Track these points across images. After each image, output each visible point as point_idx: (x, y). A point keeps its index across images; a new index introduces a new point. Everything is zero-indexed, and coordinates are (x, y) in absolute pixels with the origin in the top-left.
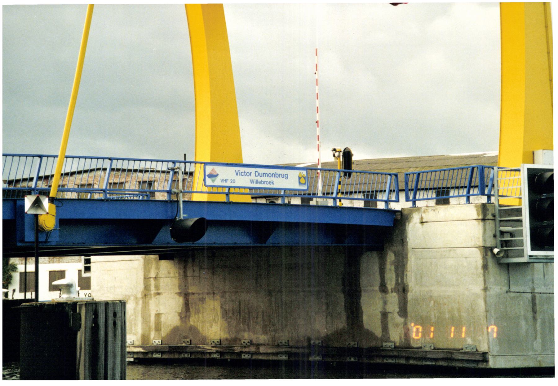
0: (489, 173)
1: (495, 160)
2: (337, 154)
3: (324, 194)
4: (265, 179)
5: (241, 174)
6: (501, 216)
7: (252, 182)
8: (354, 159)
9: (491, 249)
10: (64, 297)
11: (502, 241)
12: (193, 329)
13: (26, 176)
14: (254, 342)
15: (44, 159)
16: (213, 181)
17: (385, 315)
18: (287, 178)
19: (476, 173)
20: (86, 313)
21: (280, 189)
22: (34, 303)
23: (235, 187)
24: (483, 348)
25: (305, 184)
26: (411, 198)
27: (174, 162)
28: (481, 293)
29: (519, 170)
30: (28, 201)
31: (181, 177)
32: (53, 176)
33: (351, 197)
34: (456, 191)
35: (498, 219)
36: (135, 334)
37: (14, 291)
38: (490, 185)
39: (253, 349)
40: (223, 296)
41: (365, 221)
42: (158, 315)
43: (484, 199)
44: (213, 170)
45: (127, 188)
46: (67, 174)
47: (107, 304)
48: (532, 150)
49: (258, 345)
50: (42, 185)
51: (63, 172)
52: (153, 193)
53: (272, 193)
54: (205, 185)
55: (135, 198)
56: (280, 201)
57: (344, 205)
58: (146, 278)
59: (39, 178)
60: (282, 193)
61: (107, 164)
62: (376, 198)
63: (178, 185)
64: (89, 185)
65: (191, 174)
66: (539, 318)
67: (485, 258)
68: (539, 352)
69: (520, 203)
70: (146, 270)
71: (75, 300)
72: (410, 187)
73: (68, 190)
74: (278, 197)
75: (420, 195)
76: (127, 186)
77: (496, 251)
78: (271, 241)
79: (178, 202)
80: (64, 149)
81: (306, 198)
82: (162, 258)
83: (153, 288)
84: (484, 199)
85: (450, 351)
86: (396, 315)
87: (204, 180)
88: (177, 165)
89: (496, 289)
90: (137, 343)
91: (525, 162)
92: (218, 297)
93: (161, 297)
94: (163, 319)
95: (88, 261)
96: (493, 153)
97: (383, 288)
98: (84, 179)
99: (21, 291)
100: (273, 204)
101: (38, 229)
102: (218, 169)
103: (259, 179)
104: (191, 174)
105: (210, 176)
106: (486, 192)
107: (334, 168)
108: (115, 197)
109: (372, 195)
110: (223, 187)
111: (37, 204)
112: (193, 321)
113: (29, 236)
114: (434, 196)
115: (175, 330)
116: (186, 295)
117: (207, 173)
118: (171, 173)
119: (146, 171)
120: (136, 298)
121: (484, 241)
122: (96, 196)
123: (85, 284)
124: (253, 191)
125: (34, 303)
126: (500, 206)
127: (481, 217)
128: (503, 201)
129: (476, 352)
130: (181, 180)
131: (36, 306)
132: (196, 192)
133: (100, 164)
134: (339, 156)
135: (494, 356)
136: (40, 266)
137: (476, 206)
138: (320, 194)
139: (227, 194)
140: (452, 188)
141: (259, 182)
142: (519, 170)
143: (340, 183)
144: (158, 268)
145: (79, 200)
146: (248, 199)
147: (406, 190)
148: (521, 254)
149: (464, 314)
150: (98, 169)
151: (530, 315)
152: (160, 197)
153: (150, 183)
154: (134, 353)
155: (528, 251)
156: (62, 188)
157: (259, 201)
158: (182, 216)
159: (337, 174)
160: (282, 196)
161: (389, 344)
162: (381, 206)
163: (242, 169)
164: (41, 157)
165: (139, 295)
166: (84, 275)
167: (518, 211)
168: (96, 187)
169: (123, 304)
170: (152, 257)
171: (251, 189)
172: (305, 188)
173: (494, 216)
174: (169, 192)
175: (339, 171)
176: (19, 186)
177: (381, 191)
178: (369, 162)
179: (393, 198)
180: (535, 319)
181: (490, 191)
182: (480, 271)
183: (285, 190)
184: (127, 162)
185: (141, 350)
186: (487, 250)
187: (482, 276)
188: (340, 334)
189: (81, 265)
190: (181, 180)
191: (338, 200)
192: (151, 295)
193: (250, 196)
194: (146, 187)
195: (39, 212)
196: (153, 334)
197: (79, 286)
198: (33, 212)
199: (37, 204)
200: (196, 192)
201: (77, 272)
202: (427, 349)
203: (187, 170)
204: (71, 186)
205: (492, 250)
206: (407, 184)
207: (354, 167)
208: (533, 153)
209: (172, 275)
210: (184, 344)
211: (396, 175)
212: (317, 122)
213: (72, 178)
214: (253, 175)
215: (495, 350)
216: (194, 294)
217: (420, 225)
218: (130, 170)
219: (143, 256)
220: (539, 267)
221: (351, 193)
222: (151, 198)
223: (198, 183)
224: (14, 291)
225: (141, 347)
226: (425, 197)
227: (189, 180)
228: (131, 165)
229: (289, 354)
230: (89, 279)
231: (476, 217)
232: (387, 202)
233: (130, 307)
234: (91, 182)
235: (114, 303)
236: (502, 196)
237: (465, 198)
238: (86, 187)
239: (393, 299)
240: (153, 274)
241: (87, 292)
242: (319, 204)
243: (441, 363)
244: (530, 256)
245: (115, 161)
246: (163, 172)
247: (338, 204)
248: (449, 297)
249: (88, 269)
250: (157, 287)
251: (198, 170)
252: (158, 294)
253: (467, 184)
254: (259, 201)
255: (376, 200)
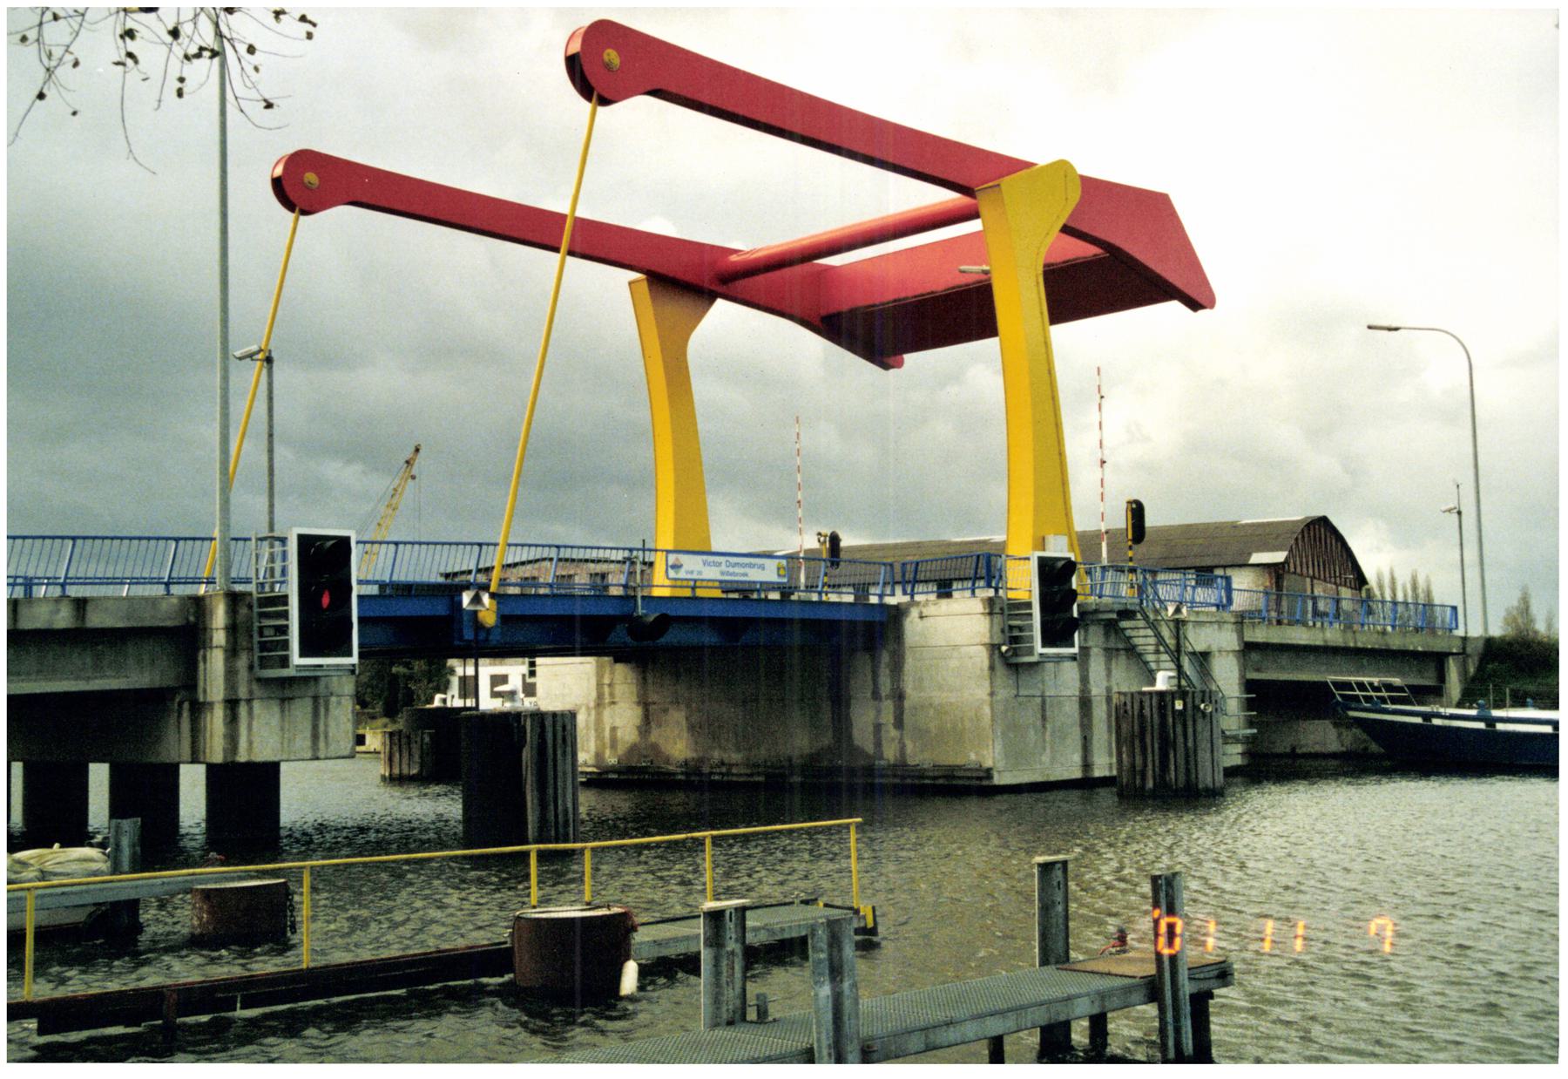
0: (996, 562)
1: (1003, 545)
2: (822, 539)
3: (807, 587)
4: (737, 570)
5: (709, 565)
6: (1009, 609)
7: (722, 573)
8: (843, 544)
9: (999, 647)
10: (508, 706)
11: (1010, 637)
12: (655, 747)
13: (464, 568)
14: (726, 762)
15: (484, 547)
16: (677, 573)
17: (878, 728)
18: (763, 569)
19: (982, 562)
20: (532, 725)
21: (754, 582)
22: (474, 712)
23: (702, 580)
24: (988, 763)
25: (784, 576)
26: (909, 591)
27: (631, 550)
28: (987, 698)
29: (1028, 559)
30: (466, 598)
31: (639, 567)
32: (493, 568)
33: (840, 590)
34: (960, 583)
35: (1006, 612)
36: (588, 752)
37: (453, 697)
38: (997, 577)
39: (724, 770)
40: (688, 706)
41: (860, 616)
42: (614, 729)
43: (991, 593)
44: (677, 559)
45: (576, 582)
46: (509, 566)
47: (554, 715)
48: (1042, 534)
49: (731, 765)
50: (482, 578)
51: (504, 563)
52: (606, 587)
53: (747, 586)
54: (668, 578)
55: (586, 593)
56: (755, 596)
57: (832, 600)
58: (600, 685)
59: (479, 571)
60: (758, 586)
61: (553, 553)
62: (868, 591)
63: (635, 578)
64: (534, 578)
65: (651, 564)
66: (1048, 726)
67: (991, 656)
68: (1047, 765)
69: (1030, 596)
70: (600, 676)
71: (519, 710)
72: (907, 579)
73: (510, 585)
74: (752, 591)
75: (920, 588)
76: (577, 579)
77: (1004, 648)
78: (744, 639)
79: (635, 597)
80: (506, 537)
81: (786, 591)
82: (617, 661)
83: (607, 695)
84: (991, 593)
85: (953, 768)
86: (891, 728)
87: (667, 570)
88: (635, 553)
89: (1003, 694)
90: (590, 762)
91: (1035, 548)
92: (683, 707)
93: (616, 707)
94: (619, 733)
95: (532, 664)
96: (999, 538)
97: (876, 695)
98: (527, 571)
99: (460, 697)
100: (746, 598)
101: (478, 626)
102: (684, 559)
103: (731, 570)
104: (651, 564)
105: (673, 567)
106: (993, 585)
107: (817, 556)
108: (563, 592)
109: (863, 588)
110: (686, 580)
111: (476, 600)
112: (653, 737)
113: (468, 634)
114: (935, 589)
115: (633, 749)
116: (645, 704)
117: (670, 563)
118: (628, 563)
119: (599, 561)
120: (588, 708)
121: (991, 637)
122: (542, 591)
123: (530, 690)
124: (723, 585)
125: (474, 712)
126: (1009, 599)
127: (987, 611)
128: (1011, 595)
129: (980, 769)
130: (638, 572)
131: (477, 716)
132: (657, 586)
133: (546, 553)
134: (825, 542)
135: (999, 772)
136: (480, 669)
137: (982, 600)
138: (802, 588)
139: (693, 588)
140: (956, 579)
141: (731, 575)
142: (1028, 559)
143: (826, 574)
144: (612, 673)
145: (522, 595)
146: (718, 594)
147: (904, 583)
148: (1031, 651)
149: (967, 724)
150: (544, 559)
151: (1039, 723)
152: (615, 591)
153: (603, 576)
154: (587, 773)
155: (1039, 649)
156: (503, 582)
157: (732, 596)
158: (640, 611)
159: (823, 564)
160: (758, 591)
161: (882, 763)
162: (874, 600)
163: (711, 558)
164: (480, 545)
165: (592, 704)
166: (529, 680)
167: (1029, 605)
168: (541, 580)
169: (573, 715)
170: (606, 659)
171: (721, 582)
172: (785, 580)
173: (1002, 609)
174: (625, 586)
175: (824, 560)
176: (457, 580)
177: (874, 584)
178: (860, 549)
179: (888, 591)
180: (1044, 726)
181: (997, 584)
182: (986, 672)
183: (761, 583)
184: (547, 549)
185: (595, 770)
186: (993, 648)
187: (988, 678)
188: (920, 845)
189: (525, 669)
190: (638, 572)
191: (824, 595)
192: (604, 704)
193: (720, 591)
194: (598, 580)
195: (478, 608)
196: (608, 752)
197: (524, 692)
198: (472, 608)
199: (476, 600)
200: (657, 586)
201: (520, 678)
202: (925, 766)
203: (646, 560)
204: (513, 580)
205: (999, 649)
206: (904, 575)
207: (843, 555)
208: (1044, 539)
209: (629, 681)
210: (644, 764)
211: (891, 565)
212: (799, 502)
213: (515, 570)
214: (724, 564)
215: (1000, 765)
216: (655, 704)
217: (918, 620)
218: (580, 560)
219: (596, 658)
220: (1050, 666)
221: (839, 586)
222: (605, 593)
223: (659, 576)
224: (453, 697)
225: (594, 766)
226: (925, 590)
227: (649, 571)
228: (580, 554)
229: (768, 776)
230: (533, 686)
231: (982, 610)
232: (881, 596)
233: (581, 719)
234: (536, 575)
235: (563, 714)
236: (1011, 589)
237: (969, 592)
238: (530, 581)
239: (888, 707)
240: (606, 681)
241: (533, 699)
242: (802, 598)
243: (941, 781)
244: (1041, 654)
245: (562, 550)
246: (619, 562)
247: (824, 598)
248: (951, 704)
249: (532, 674)
250: (612, 695)
251: (659, 560)
252: (614, 703)
253: (972, 575)
254: (732, 596)
255: (869, 594)
